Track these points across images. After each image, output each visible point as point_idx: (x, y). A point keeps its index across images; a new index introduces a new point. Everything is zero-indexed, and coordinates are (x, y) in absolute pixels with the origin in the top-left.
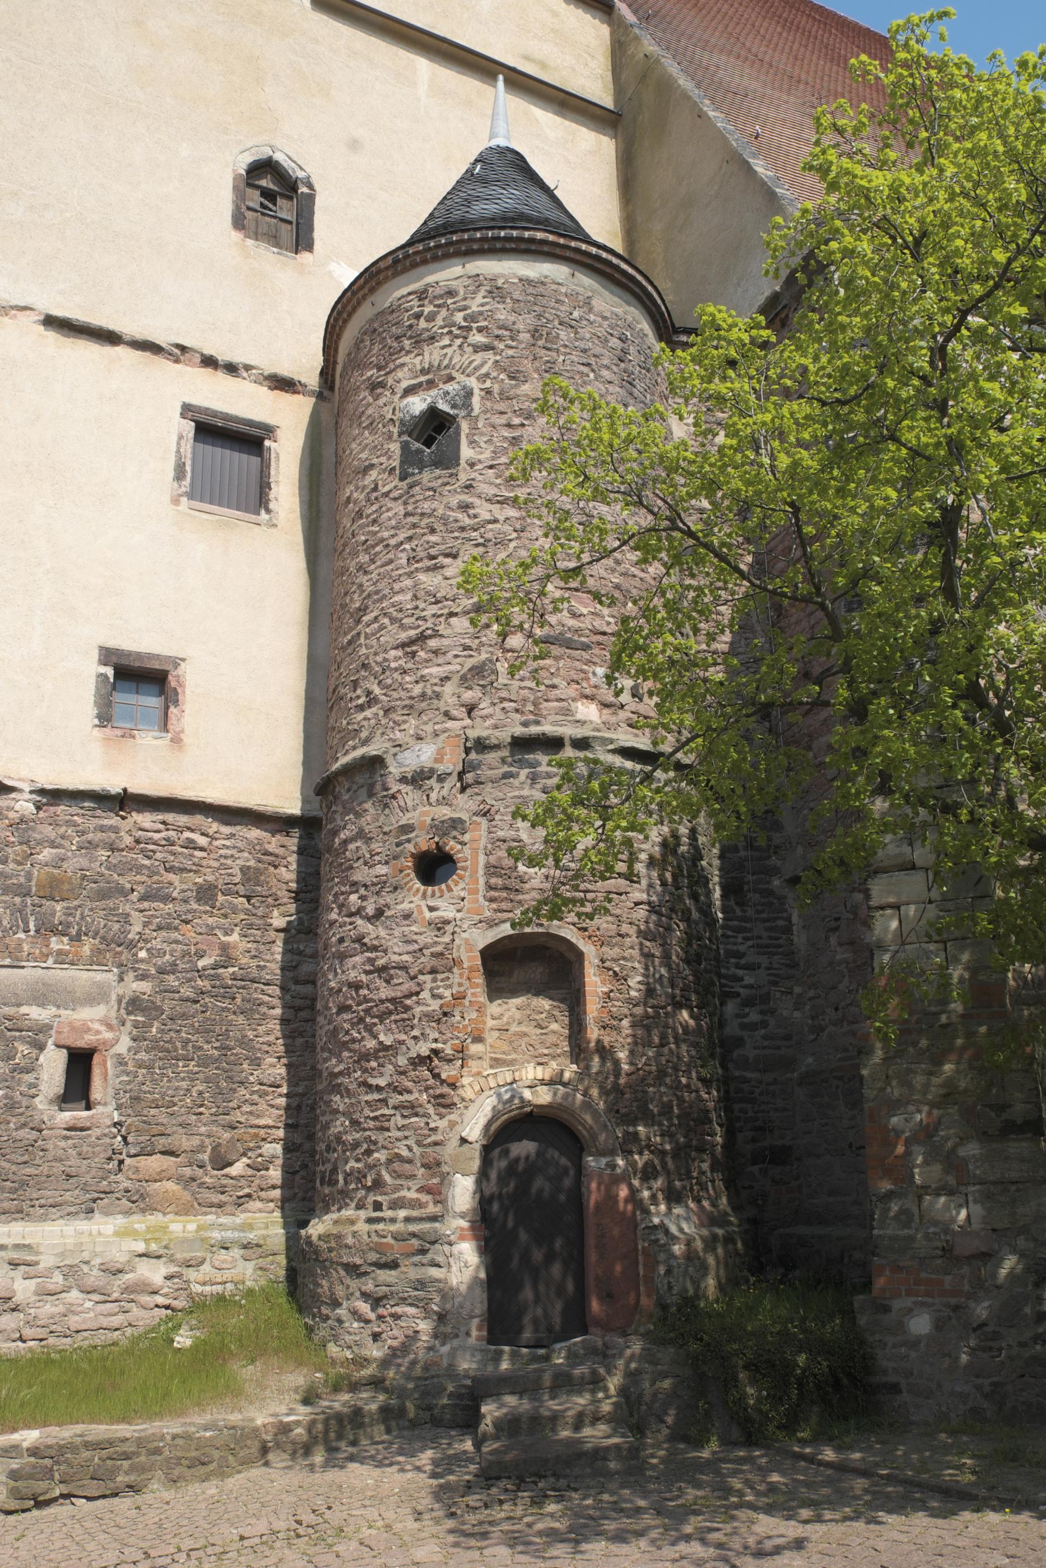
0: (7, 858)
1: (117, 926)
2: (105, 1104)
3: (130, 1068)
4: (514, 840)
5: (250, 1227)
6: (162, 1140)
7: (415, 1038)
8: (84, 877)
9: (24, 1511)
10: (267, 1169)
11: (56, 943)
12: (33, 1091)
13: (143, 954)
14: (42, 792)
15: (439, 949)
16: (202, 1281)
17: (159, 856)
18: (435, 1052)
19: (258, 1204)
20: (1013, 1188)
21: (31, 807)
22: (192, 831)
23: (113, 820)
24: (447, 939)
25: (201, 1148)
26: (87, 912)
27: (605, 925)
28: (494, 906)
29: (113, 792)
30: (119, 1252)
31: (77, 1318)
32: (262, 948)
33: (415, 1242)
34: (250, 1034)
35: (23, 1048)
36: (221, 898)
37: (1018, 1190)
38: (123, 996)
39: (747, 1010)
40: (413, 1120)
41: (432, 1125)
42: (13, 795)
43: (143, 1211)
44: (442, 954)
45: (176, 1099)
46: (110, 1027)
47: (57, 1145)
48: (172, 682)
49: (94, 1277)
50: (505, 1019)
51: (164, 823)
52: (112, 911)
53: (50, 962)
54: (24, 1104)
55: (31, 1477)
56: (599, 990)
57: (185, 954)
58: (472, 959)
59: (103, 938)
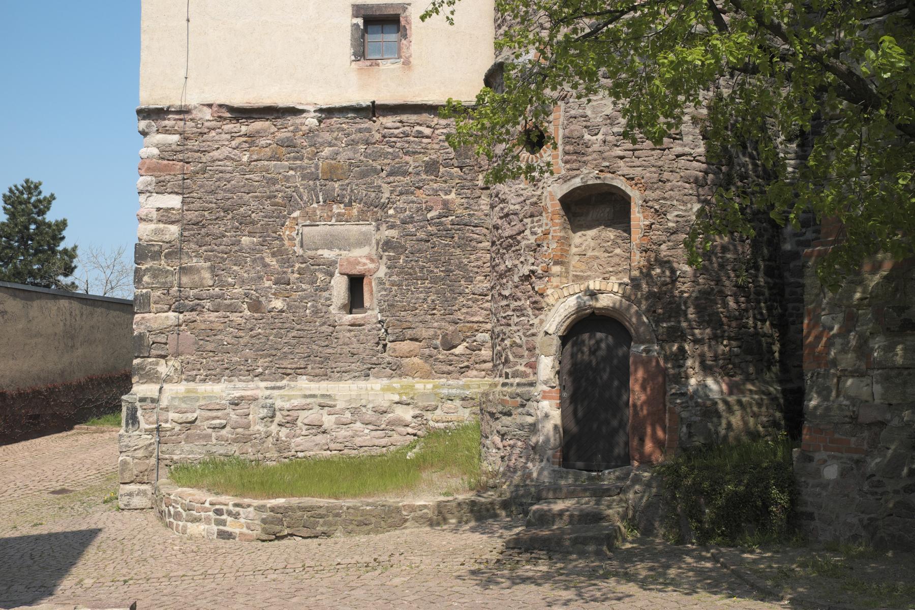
0: (303, 156)
1: (373, 195)
2: (373, 309)
3: (387, 286)
4: (582, 116)
5: (468, 387)
6: (409, 332)
7: (522, 262)
8: (350, 164)
9: (270, 541)
10: (480, 350)
11: (337, 209)
12: (328, 302)
13: (391, 212)
14: (321, 110)
15: (534, 199)
16: (436, 419)
17: (398, 145)
18: (533, 272)
19: (475, 373)
20: (906, 372)
21: (315, 122)
22: (421, 125)
23: (367, 124)
24: (539, 192)
25: (435, 336)
26: (354, 187)
27: (648, 175)
28: (568, 166)
29: (364, 105)
30: (384, 401)
31: (360, 439)
32: (471, 202)
33: (519, 399)
34: (465, 261)
35: (321, 276)
36: (442, 170)
37: (910, 374)
38: (380, 240)
39: (804, 230)
40: (522, 318)
41: (531, 322)
42: (304, 115)
43: (400, 376)
44: (536, 203)
45: (417, 305)
46: (372, 260)
47: (344, 336)
48: (403, 22)
49: (369, 415)
50: (583, 247)
51: (401, 122)
52: (370, 185)
53: (334, 220)
54: (324, 310)
55: (272, 523)
56: (641, 223)
57: (419, 210)
58: (553, 205)
59: (365, 203)
